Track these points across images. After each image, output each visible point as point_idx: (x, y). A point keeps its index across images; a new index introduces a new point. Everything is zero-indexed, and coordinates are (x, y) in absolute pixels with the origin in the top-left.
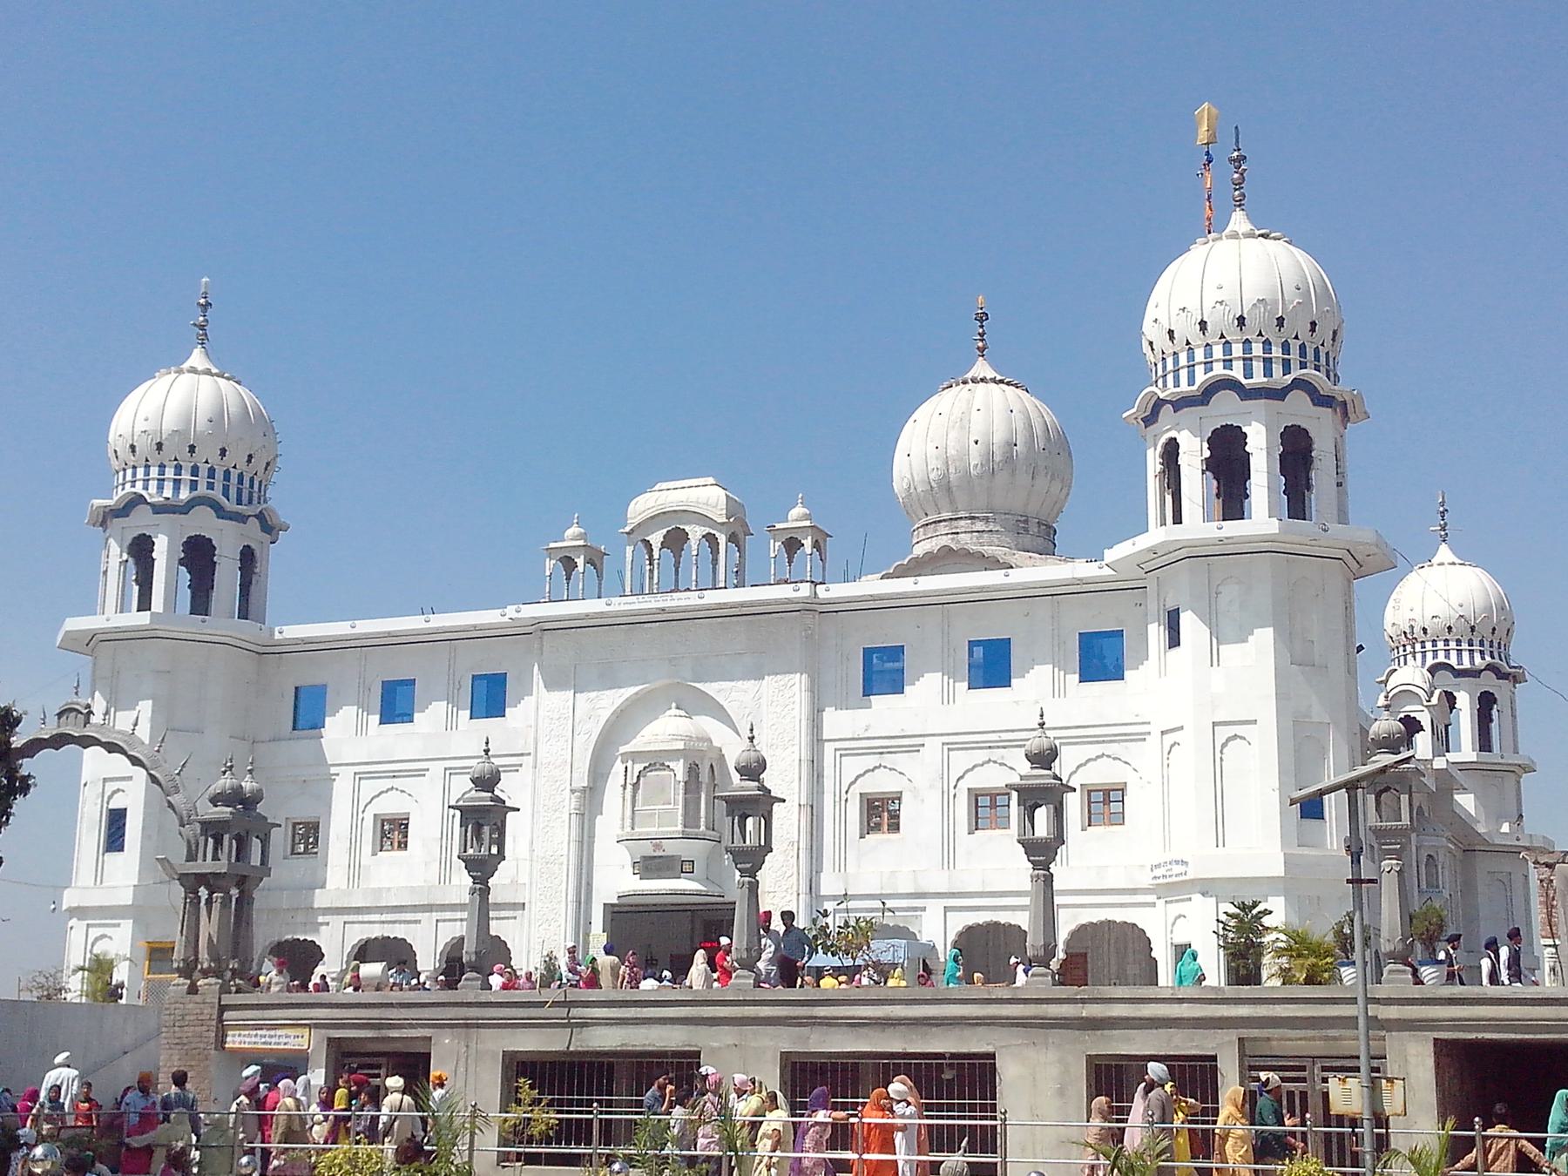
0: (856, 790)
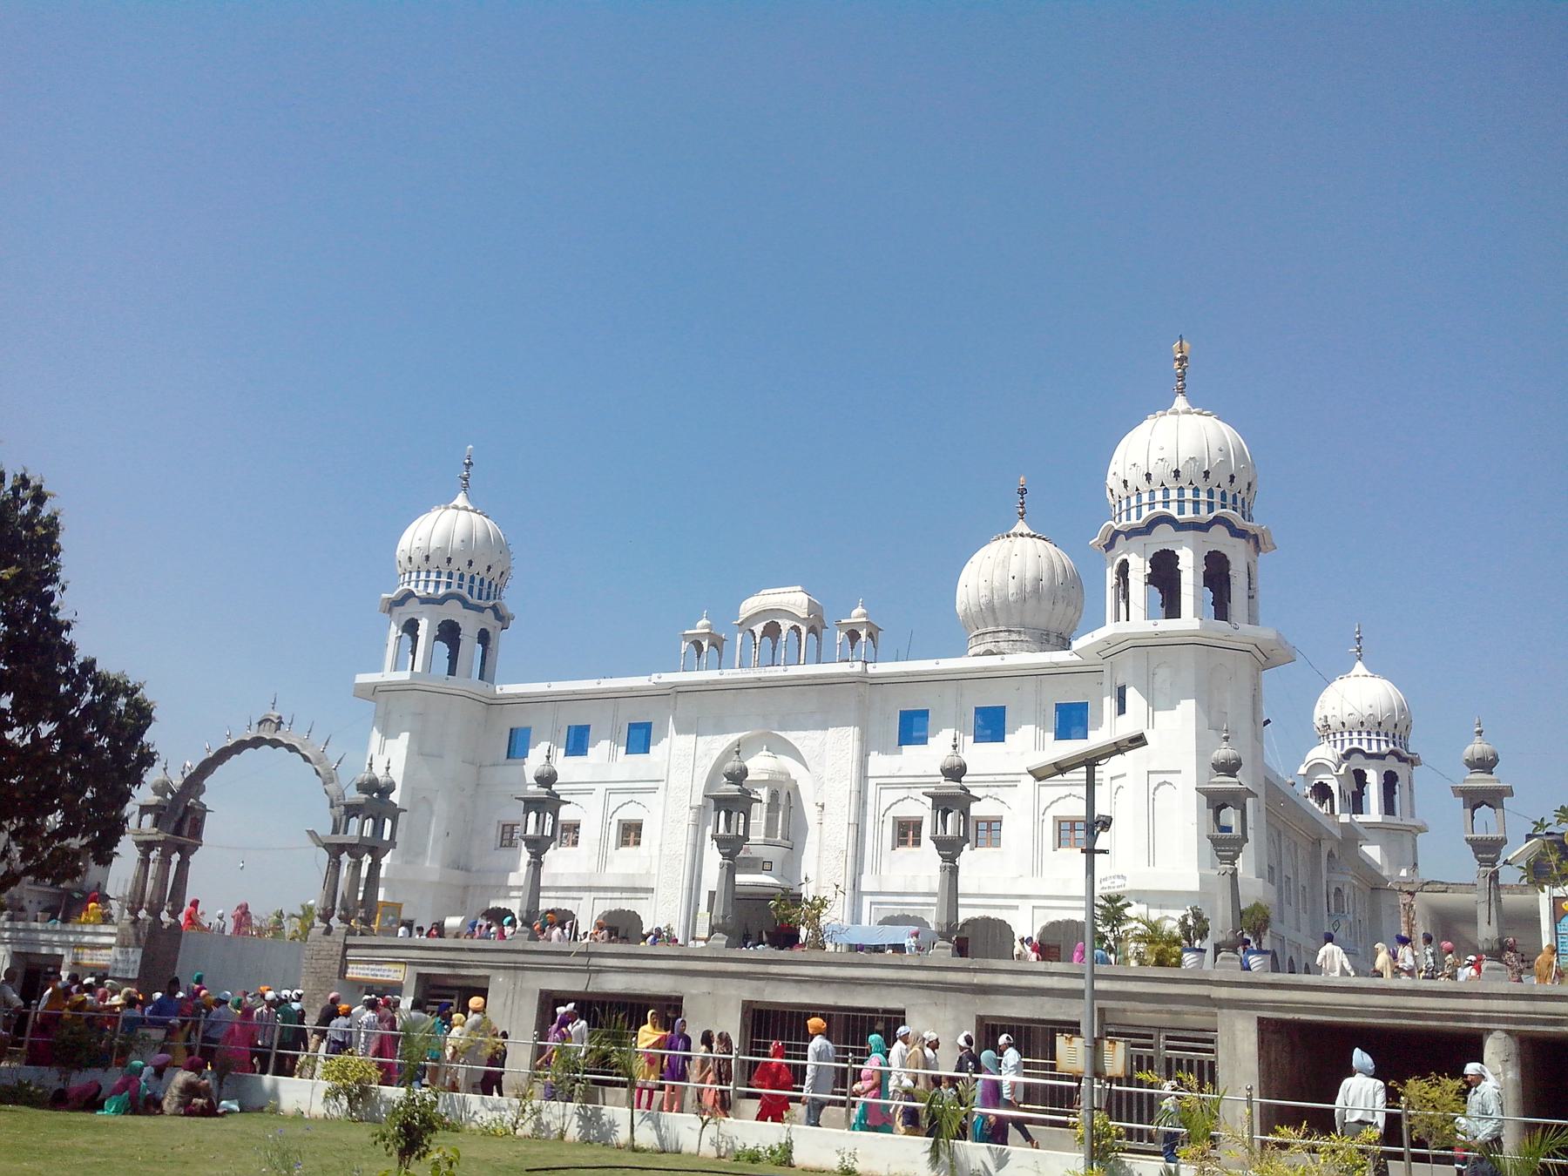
0: (891, 813)
